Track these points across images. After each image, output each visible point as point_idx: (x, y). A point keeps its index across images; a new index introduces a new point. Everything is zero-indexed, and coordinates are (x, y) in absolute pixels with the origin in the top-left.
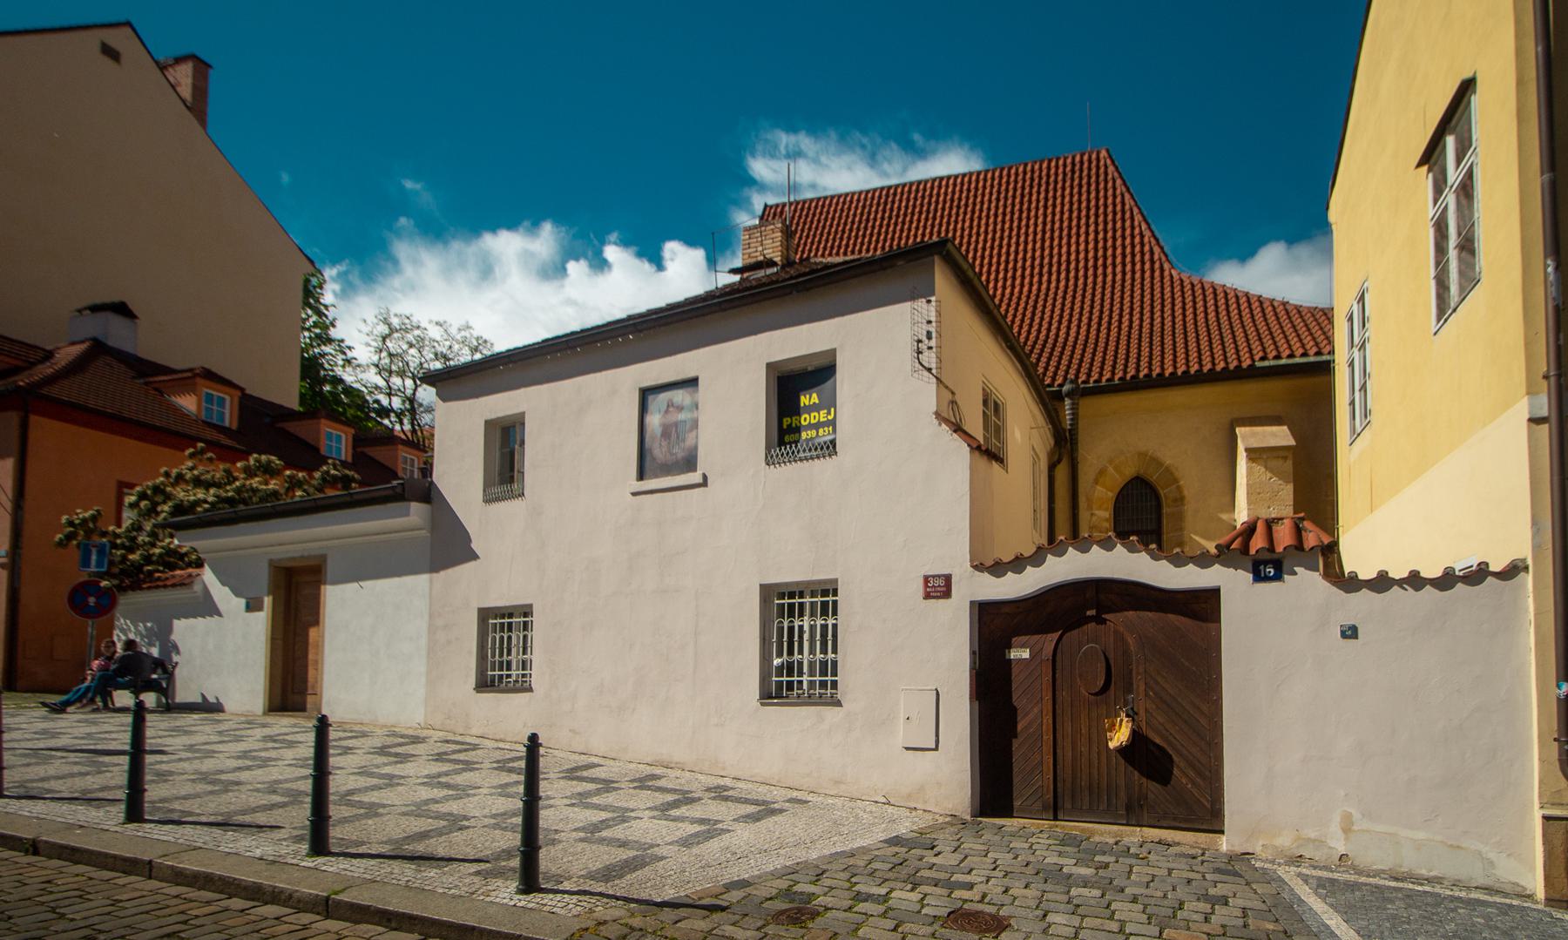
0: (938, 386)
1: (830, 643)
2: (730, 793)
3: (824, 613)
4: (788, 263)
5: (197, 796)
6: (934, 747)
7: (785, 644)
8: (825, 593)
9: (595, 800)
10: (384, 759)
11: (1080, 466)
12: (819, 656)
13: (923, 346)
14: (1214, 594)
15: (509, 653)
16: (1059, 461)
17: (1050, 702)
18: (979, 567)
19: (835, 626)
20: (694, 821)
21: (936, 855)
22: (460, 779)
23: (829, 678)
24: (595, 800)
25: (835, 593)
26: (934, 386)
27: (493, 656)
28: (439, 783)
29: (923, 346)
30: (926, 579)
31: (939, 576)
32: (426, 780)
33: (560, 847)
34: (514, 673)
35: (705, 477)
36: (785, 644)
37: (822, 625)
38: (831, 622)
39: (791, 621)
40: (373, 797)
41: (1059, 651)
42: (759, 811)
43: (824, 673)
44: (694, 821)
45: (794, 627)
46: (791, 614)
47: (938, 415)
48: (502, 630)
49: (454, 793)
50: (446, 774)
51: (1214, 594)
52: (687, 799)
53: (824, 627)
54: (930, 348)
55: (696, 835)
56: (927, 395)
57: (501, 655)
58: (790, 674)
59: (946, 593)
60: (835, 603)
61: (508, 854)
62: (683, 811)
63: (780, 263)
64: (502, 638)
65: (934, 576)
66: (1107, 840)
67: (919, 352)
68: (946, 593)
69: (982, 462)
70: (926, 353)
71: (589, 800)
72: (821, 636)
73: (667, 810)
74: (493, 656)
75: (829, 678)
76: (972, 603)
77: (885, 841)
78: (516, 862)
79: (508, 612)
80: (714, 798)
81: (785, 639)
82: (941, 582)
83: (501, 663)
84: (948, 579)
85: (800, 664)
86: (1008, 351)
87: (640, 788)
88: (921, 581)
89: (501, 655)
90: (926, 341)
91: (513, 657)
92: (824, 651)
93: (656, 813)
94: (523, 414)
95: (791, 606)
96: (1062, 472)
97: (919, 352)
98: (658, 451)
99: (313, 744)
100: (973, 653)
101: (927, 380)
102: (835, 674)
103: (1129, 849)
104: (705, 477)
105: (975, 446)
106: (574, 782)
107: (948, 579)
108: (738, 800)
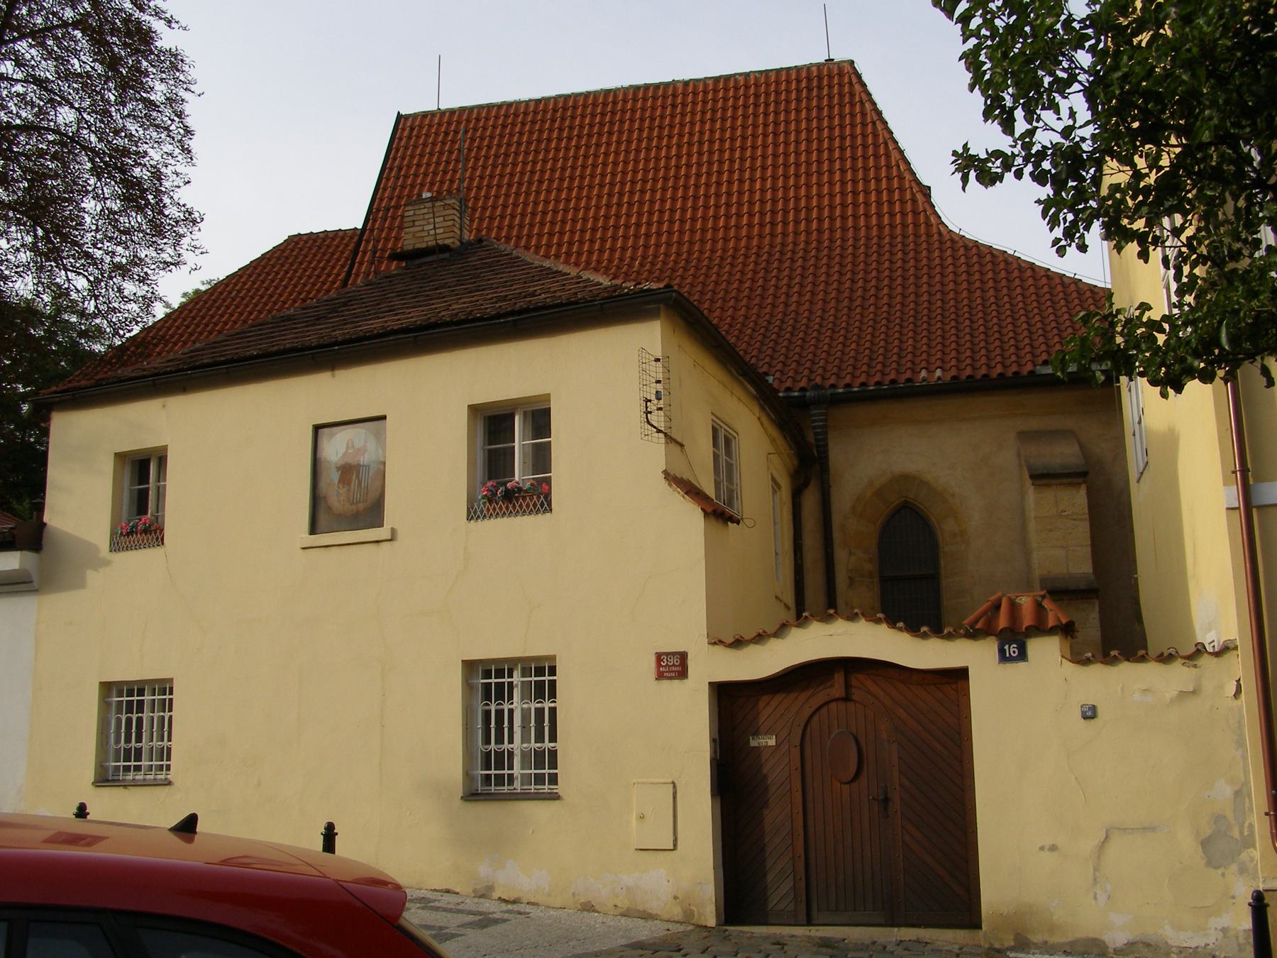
0: (667, 443)
2: (436, 904)
6: (672, 848)
7: (134, 735)
8: (540, 671)
11: (833, 490)
13: (651, 407)
14: (959, 676)
15: (139, 739)
16: (806, 484)
17: (800, 793)
18: (716, 642)
23: (546, 771)
25: (553, 671)
26: (663, 440)
27: (118, 741)
29: (651, 407)
30: (659, 657)
31: (674, 654)
35: (393, 531)
36: (123, 735)
37: (550, 708)
39: (487, 704)
41: (808, 736)
43: (500, 765)
47: (667, 475)
48: (130, 710)
51: (959, 676)
54: (660, 409)
56: (656, 454)
57: (128, 740)
64: (129, 721)
65: (667, 654)
66: (601, 280)
68: (682, 673)
69: (716, 526)
74: (118, 741)
75: (546, 771)
76: (710, 684)
77: (626, 946)
79: (138, 688)
81: (493, 725)
82: (676, 661)
83: (127, 752)
84: (683, 656)
85: (511, 754)
86: (741, 378)
88: (653, 659)
89: (128, 740)
90: (656, 401)
91: (145, 744)
92: (500, 740)
96: (810, 500)
97: (647, 413)
98: (336, 497)
100: (713, 741)
102: (169, 759)
103: (885, 947)
104: (393, 531)
105: (709, 510)
107: (683, 656)
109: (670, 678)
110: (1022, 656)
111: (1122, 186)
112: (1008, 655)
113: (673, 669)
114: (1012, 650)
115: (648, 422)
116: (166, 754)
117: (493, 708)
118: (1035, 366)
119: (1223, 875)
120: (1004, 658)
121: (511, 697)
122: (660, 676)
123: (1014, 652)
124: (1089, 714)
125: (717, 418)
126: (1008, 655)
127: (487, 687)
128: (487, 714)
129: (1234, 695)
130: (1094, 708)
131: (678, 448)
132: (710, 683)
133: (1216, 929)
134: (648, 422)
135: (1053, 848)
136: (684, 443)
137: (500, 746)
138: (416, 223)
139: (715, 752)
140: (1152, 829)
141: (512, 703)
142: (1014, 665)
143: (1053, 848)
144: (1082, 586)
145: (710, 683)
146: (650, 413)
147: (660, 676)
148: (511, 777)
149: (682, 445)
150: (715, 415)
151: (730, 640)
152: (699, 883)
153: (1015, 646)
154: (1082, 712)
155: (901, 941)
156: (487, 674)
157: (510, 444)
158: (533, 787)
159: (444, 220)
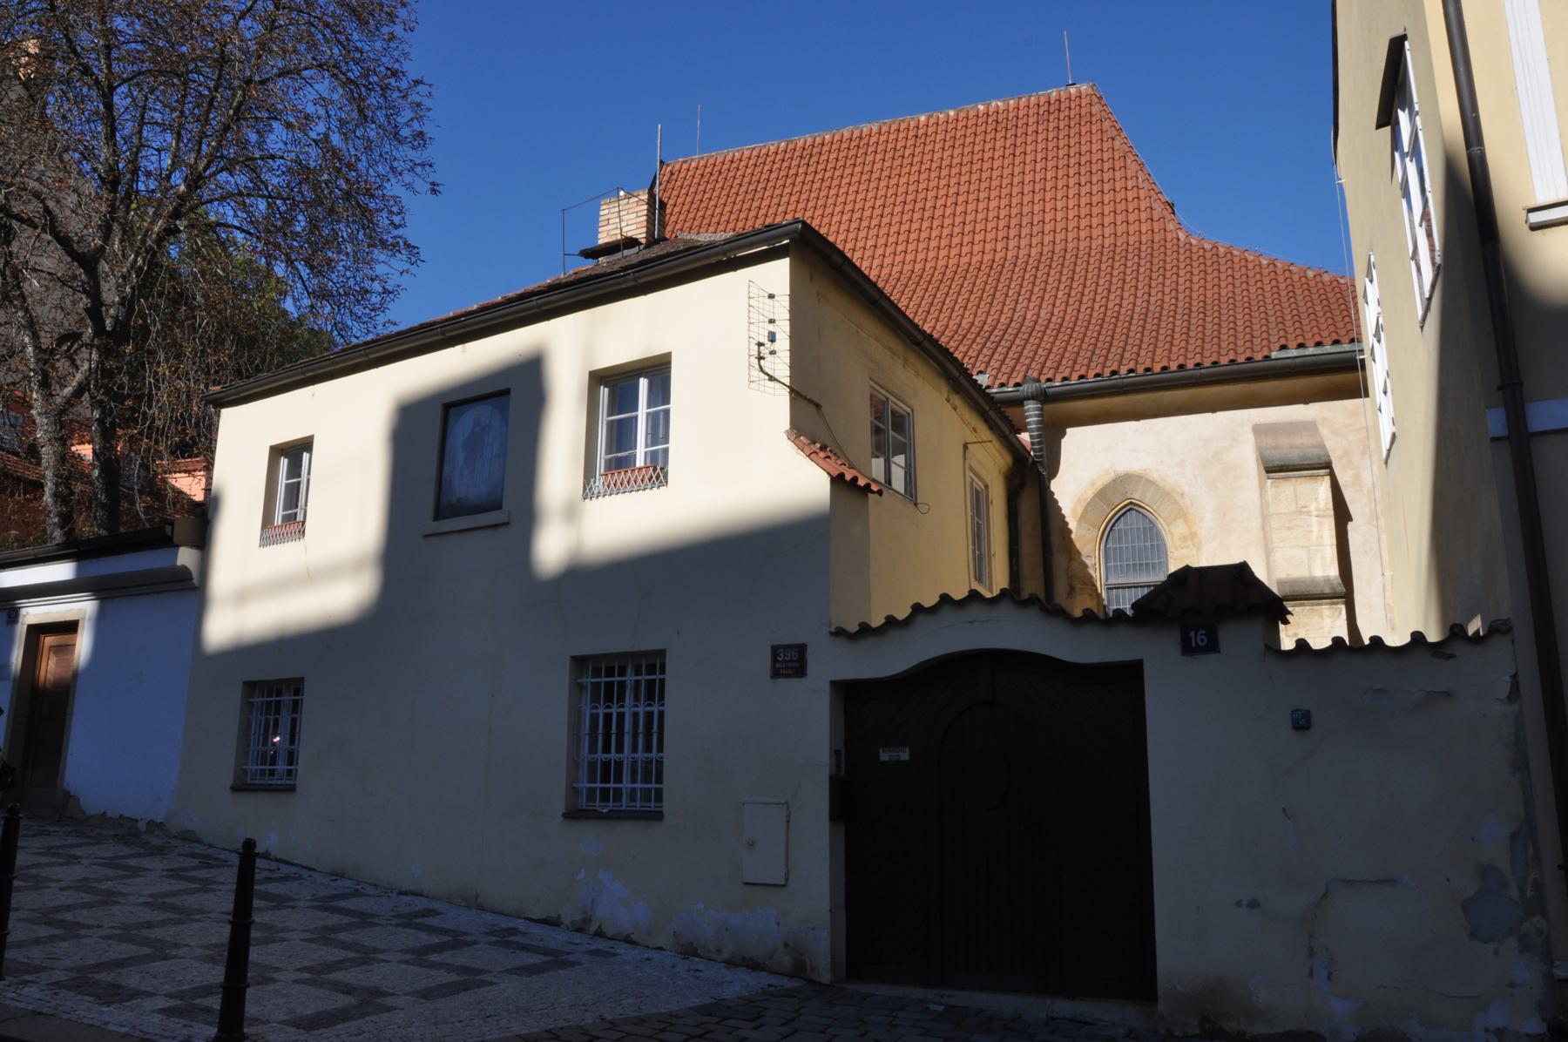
1: (655, 737)
2: (519, 939)
3: (650, 697)
4: (652, 241)
5: (37, 942)
6: (783, 882)
9: (342, 936)
10: (111, 872)
12: (640, 755)
16: (1022, 486)
19: (661, 714)
20: (451, 968)
21: (755, 1028)
22: (191, 901)
24: (342, 936)
28: (164, 903)
30: (775, 651)
32: (150, 900)
33: (272, 987)
34: (626, 785)
38: (614, 711)
40: (166, 933)
42: (545, 962)
44: (451, 968)
45: (598, 715)
46: (609, 699)
49: (177, 916)
50: (175, 894)
52: (457, 941)
53: (608, 717)
54: (773, 353)
55: (447, 985)
58: (606, 779)
59: (800, 671)
60: (662, 682)
61: (207, 991)
62: (447, 957)
63: (643, 241)
67: (760, 358)
68: (800, 671)
70: (769, 358)
71: (333, 936)
72: (617, 728)
73: (426, 953)
77: (690, 1008)
78: (215, 1003)
80: (492, 944)
81: (600, 730)
84: (801, 649)
85: (619, 765)
87: (405, 926)
88: (769, 652)
93: (409, 957)
94: (669, 354)
95: (609, 685)
97: (760, 358)
99: (234, 887)
101: (772, 391)
102: (659, 780)
106: (325, 914)
107: (801, 649)
108: (524, 948)
109: (788, 676)
110: (1212, 646)
111: (1481, 634)
112: (1194, 644)
113: (791, 664)
114: (1199, 638)
115: (761, 369)
116: (653, 772)
117: (601, 711)
118: (1271, 351)
119: (1496, 952)
120: (1188, 649)
121: (621, 698)
122: (776, 674)
123: (1202, 640)
124: (1302, 722)
125: (877, 383)
126: (1194, 644)
127: (596, 686)
128: (594, 718)
129: (1508, 697)
130: (1307, 715)
131: (812, 408)
132: (834, 684)
133: (1487, 1030)
134: (761, 369)
135: (1254, 904)
136: (821, 403)
137: (594, 756)
138: (611, 221)
139: (838, 767)
140: (1391, 882)
141: (623, 706)
142: (1202, 658)
143: (1254, 904)
144: (1327, 590)
145: (834, 684)
146: (763, 358)
147: (776, 674)
148: (618, 792)
149: (818, 406)
150: (873, 381)
151: (854, 628)
152: (813, 929)
153: (1204, 632)
154: (1293, 719)
155: (1053, 1018)
156: (597, 673)
157: (633, 414)
158: (652, 804)
159: (637, 217)
